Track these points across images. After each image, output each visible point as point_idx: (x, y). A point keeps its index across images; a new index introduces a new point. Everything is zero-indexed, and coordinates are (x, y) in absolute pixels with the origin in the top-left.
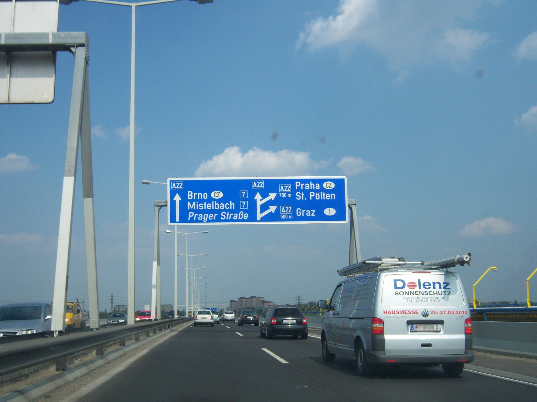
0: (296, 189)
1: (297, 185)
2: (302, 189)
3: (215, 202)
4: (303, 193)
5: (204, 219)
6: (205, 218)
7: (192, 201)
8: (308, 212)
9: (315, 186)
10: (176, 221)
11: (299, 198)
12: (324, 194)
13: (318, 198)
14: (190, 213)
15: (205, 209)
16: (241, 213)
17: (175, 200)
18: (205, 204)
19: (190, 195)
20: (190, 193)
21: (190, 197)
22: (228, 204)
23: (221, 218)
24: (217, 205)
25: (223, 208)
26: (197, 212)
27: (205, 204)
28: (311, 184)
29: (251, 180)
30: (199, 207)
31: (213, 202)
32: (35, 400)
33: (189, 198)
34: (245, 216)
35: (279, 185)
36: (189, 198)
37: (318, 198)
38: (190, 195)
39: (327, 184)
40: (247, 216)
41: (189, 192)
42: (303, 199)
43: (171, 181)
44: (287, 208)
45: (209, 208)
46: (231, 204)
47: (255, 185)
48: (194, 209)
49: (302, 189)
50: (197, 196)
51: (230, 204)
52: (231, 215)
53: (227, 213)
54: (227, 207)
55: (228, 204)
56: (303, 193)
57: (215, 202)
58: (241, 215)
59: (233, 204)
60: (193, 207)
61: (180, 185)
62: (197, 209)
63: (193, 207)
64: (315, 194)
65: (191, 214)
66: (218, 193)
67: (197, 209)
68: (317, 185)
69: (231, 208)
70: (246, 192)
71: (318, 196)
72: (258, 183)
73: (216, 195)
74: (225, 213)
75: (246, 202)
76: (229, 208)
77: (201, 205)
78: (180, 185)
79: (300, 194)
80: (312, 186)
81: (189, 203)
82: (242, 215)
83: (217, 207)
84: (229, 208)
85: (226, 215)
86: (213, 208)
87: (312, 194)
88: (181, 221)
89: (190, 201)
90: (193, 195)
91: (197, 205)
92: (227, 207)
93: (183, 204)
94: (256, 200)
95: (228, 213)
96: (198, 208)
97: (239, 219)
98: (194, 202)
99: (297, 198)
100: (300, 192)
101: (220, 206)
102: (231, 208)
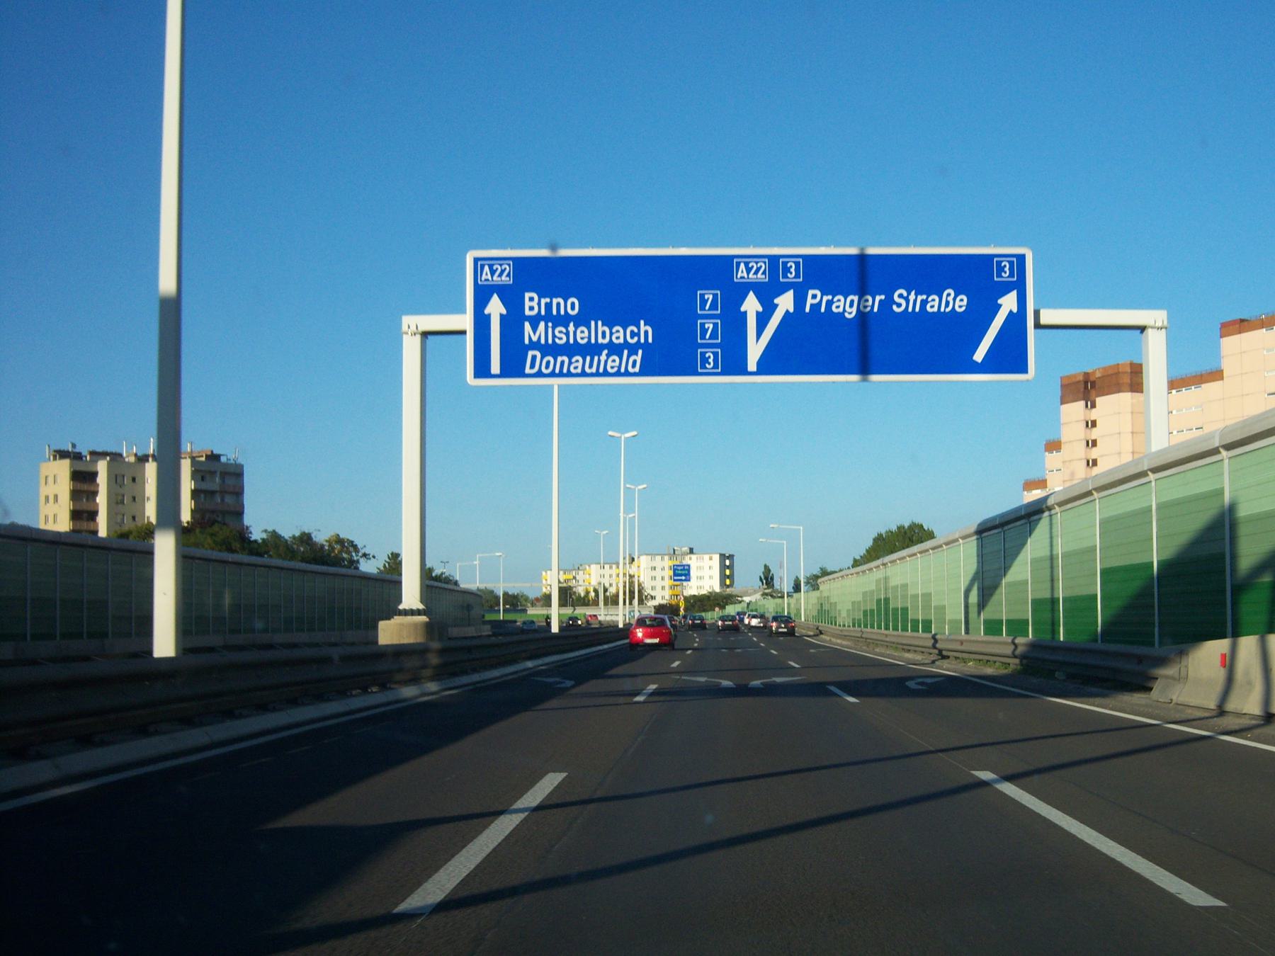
0: (640, 352)
5: (847, 308)
6: (851, 305)
15: (571, 341)
16: (949, 295)
18: (571, 328)
20: (531, 299)
22: (636, 330)
23: (895, 307)
24: (604, 333)
25: (621, 341)
26: (551, 350)
27: (571, 328)
29: (731, 258)
30: (554, 336)
31: (593, 323)
32: (858, 563)
33: (527, 312)
36: (527, 312)
40: (965, 302)
41: (527, 295)
43: (476, 260)
44: (753, 267)
45: (582, 338)
46: (643, 327)
47: (742, 272)
48: (543, 341)
50: (549, 306)
51: (639, 330)
52: (920, 298)
53: (909, 294)
54: (632, 337)
55: (636, 330)
57: (600, 323)
58: (949, 299)
60: (539, 338)
62: (550, 341)
63: (539, 338)
65: (814, 297)
67: (550, 341)
69: (642, 341)
70: (715, 296)
72: (750, 265)
74: (905, 294)
75: (715, 325)
76: (636, 339)
77: (560, 332)
78: (503, 271)
81: (527, 326)
82: (950, 299)
84: (636, 339)
86: (593, 341)
89: (530, 319)
91: (550, 330)
92: (632, 337)
93: (512, 323)
94: (745, 313)
95: (913, 293)
96: (553, 340)
97: (942, 310)
98: (542, 324)
100: (906, 290)
101: (611, 334)
102: (642, 341)
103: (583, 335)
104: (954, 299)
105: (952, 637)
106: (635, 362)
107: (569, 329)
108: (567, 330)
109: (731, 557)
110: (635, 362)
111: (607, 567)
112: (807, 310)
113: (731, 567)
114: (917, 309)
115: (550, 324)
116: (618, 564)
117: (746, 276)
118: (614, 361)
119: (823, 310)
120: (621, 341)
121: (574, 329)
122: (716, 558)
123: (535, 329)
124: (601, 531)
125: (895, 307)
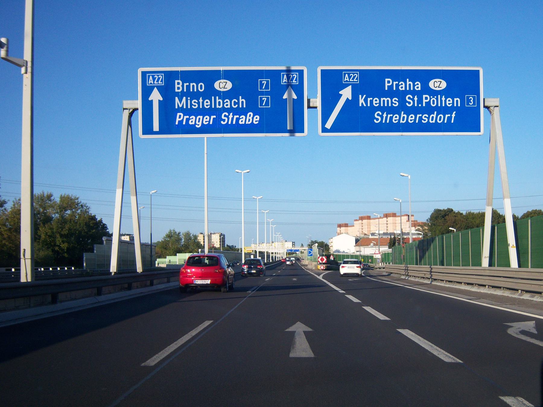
1: (388, 83)
2: (394, 89)
3: (217, 97)
4: (416, 97)
5: (197, 123)
7: (181, 96)
8: (402, 84)
9: (414, 86)
10: (154, 130)
11: (409, 103)
12: (443, 99)
13: (434, 103)
14: (178, 114)
17: (342, 95)
18: (201, 100)
19: (178, 86)
20: (178, 84)
21: (178, 88)
22: (237, 101)
23: (222, 122)
24: (219, 102)
25: (229, 106)
28: (408, 83)
30: (191, 104)
31: (213, 97)
33: (176, 90)
34: (255, 119)
35: (343, 83)
36: (176, 90)
37: (434, 103)
38: (178, 86)
39: (435, 83)
40: (258, 119)
42: (416, 105)
44: (352, 76)
46: (241, 100)
47: (346, 78)
48: (185, 107)
49: (394, 89)
50: (188, 87)
52: (235, 117)
54: (235, 105)
55: (237, 101)
56: (416, 97)
57: (217, 97)
59: (244, 100)
61: (354, 77)
62: (390, 105)
64: (430, 99)
66: (439, 82)
67: (390, 105)
68: (418, 84)
69: (240, 106)
70: (267, 82)
71: (433, 101)
73: (437, 84)
76: (237, 106)
77: (195, 102)
78: (354, 77)
79: (412, 97)
80: (410, 85)
81: (177, 99)
83: (219, 105)
84: (237, 106)
85: (228, 117)
87: (426, 98)
88: (162, 131)
90: (183, 86)
91: (189, 101)
92: (235, 105)
95: (231, 114)
99: (407, 104)
101: (224, 103)
102: (240, 106)
103: (207, 104)
104: (253, 118)
105: (229, 278)
106: (180, 117)
107: (200, 101)
108: (198, 101)
109: (294, 242)
110: (180, 117)
111: (267, 244)
112: (177, 123)
113: (294, 245)
114: (234, 123)
115: (189, 98)
116: (270, 243)
117: (348, 80)
118: (412, 117)
119: (184, 123)
120: (229, 106)
121: (202, 101)
122: (291, 243)
123: (181, 101)
124: (270, 220)
125: (222, 122)
